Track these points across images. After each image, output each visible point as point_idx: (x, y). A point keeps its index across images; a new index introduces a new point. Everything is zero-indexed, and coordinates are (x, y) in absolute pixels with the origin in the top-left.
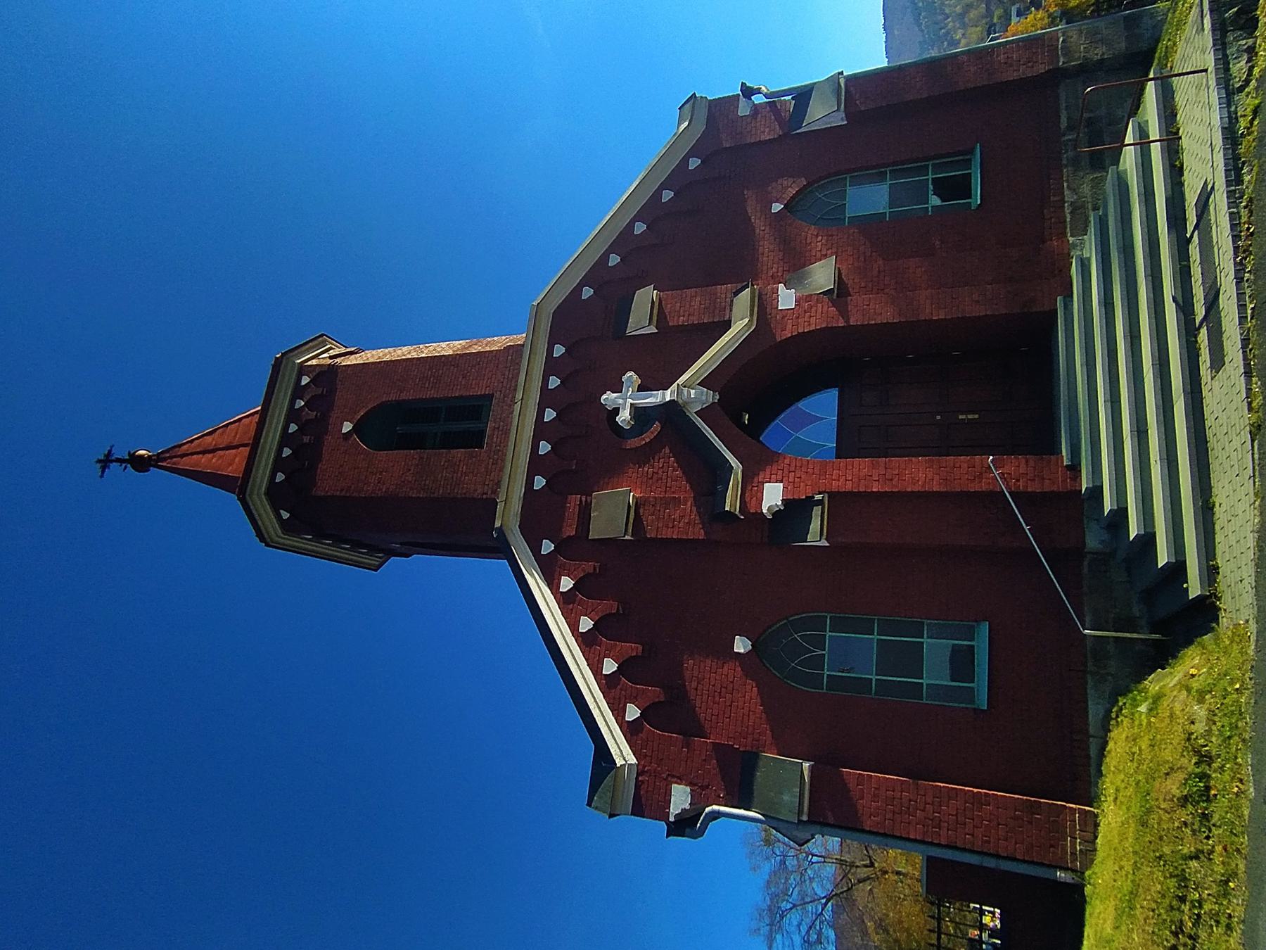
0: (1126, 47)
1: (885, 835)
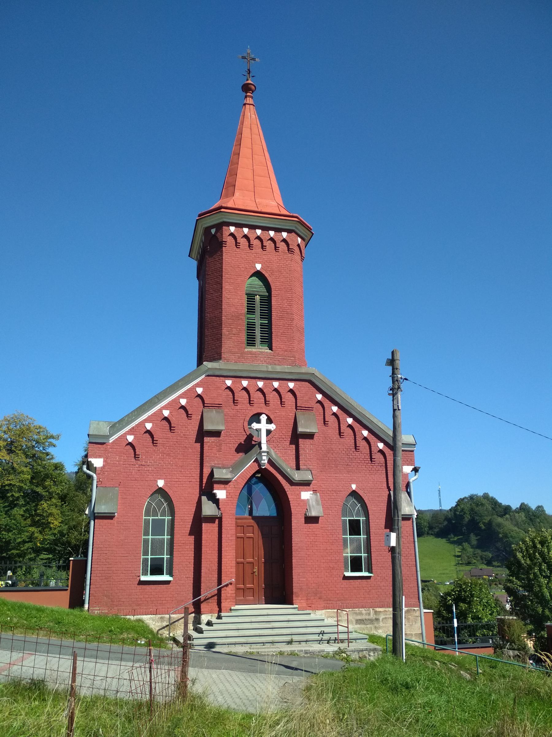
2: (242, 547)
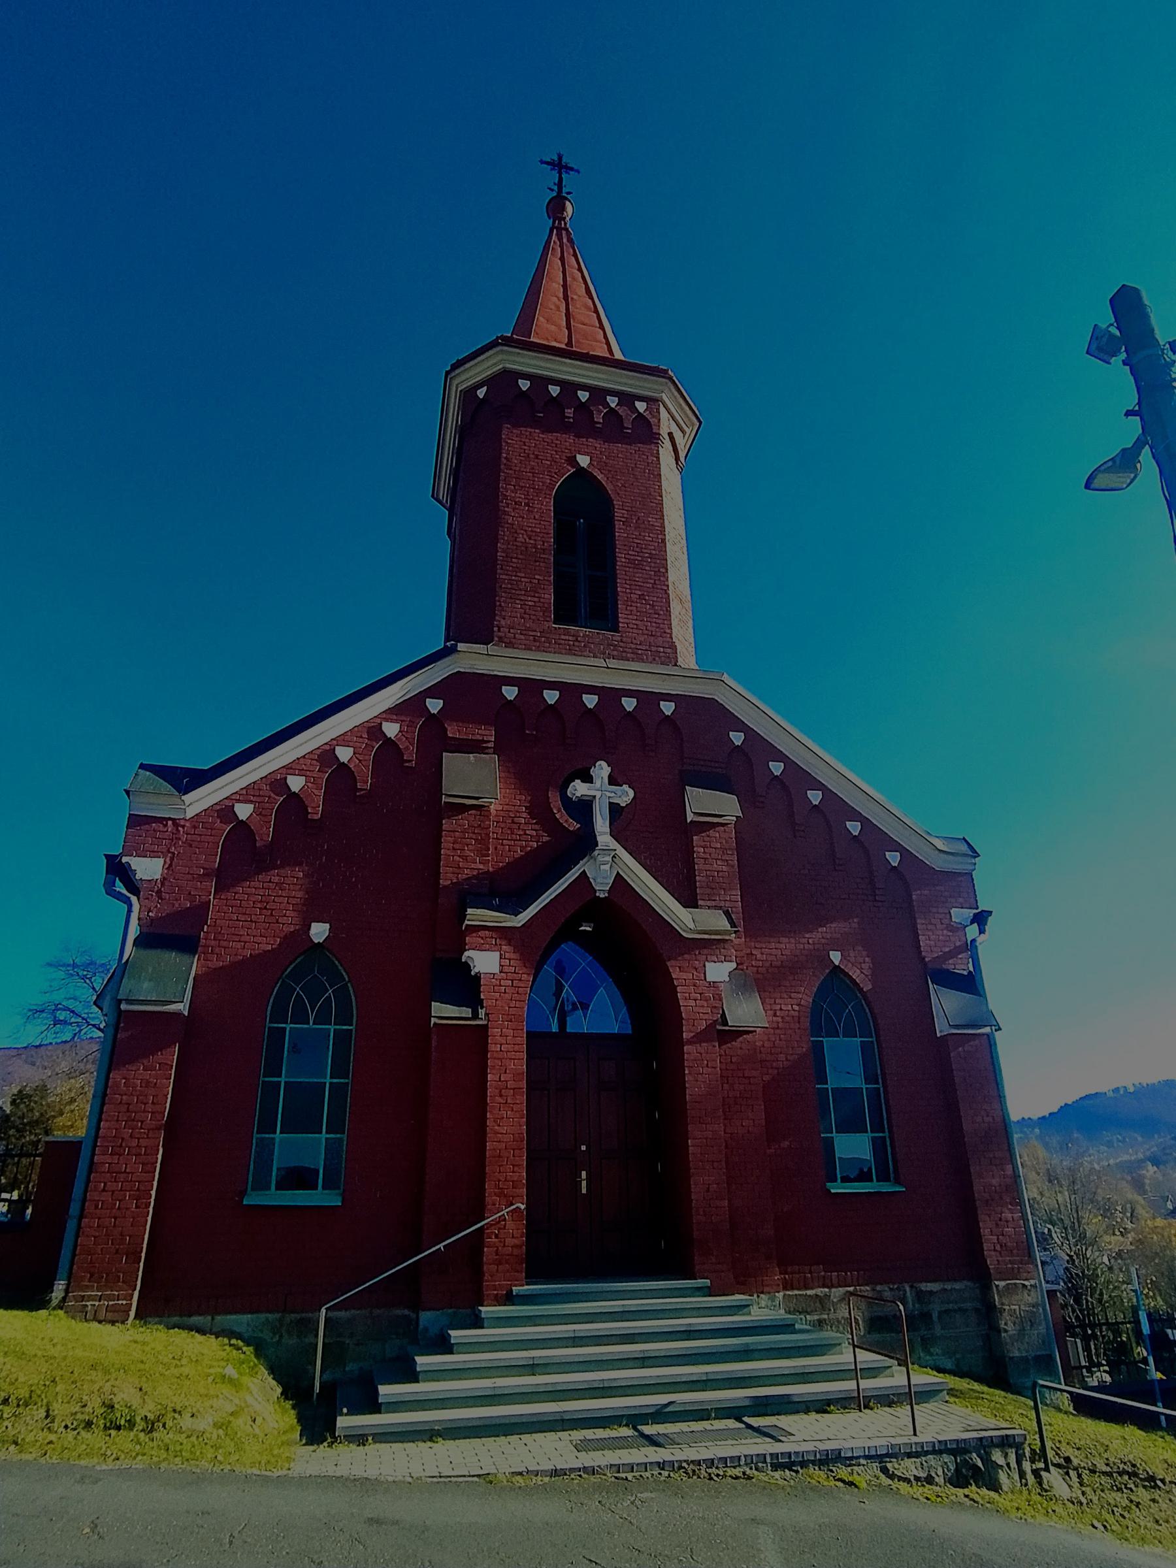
0: (1013, 1357)
1: (105, 1095)
2: (737, 695)
